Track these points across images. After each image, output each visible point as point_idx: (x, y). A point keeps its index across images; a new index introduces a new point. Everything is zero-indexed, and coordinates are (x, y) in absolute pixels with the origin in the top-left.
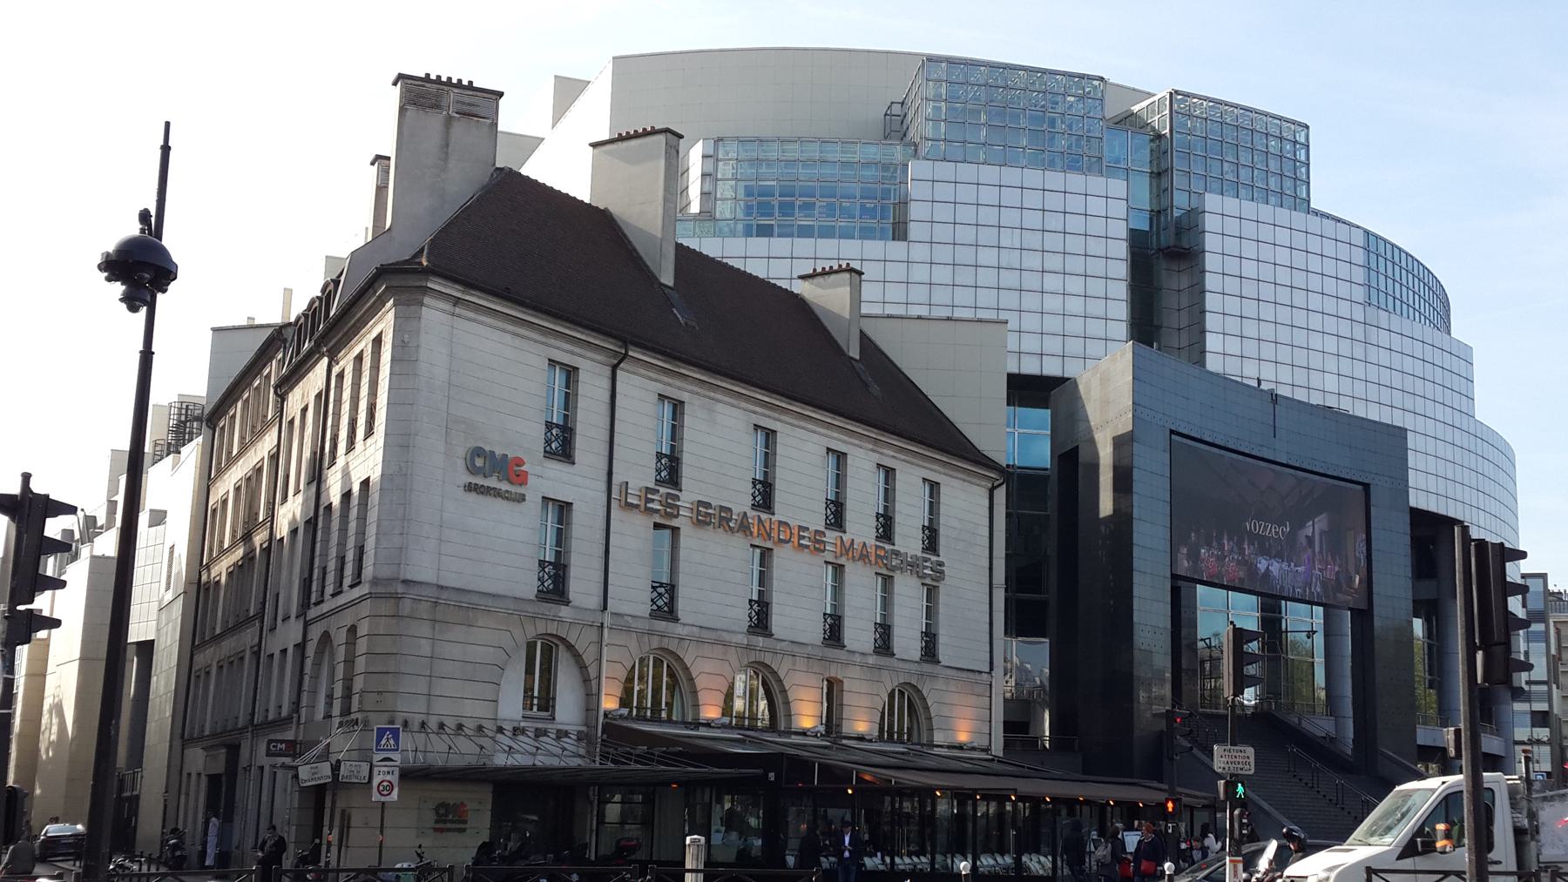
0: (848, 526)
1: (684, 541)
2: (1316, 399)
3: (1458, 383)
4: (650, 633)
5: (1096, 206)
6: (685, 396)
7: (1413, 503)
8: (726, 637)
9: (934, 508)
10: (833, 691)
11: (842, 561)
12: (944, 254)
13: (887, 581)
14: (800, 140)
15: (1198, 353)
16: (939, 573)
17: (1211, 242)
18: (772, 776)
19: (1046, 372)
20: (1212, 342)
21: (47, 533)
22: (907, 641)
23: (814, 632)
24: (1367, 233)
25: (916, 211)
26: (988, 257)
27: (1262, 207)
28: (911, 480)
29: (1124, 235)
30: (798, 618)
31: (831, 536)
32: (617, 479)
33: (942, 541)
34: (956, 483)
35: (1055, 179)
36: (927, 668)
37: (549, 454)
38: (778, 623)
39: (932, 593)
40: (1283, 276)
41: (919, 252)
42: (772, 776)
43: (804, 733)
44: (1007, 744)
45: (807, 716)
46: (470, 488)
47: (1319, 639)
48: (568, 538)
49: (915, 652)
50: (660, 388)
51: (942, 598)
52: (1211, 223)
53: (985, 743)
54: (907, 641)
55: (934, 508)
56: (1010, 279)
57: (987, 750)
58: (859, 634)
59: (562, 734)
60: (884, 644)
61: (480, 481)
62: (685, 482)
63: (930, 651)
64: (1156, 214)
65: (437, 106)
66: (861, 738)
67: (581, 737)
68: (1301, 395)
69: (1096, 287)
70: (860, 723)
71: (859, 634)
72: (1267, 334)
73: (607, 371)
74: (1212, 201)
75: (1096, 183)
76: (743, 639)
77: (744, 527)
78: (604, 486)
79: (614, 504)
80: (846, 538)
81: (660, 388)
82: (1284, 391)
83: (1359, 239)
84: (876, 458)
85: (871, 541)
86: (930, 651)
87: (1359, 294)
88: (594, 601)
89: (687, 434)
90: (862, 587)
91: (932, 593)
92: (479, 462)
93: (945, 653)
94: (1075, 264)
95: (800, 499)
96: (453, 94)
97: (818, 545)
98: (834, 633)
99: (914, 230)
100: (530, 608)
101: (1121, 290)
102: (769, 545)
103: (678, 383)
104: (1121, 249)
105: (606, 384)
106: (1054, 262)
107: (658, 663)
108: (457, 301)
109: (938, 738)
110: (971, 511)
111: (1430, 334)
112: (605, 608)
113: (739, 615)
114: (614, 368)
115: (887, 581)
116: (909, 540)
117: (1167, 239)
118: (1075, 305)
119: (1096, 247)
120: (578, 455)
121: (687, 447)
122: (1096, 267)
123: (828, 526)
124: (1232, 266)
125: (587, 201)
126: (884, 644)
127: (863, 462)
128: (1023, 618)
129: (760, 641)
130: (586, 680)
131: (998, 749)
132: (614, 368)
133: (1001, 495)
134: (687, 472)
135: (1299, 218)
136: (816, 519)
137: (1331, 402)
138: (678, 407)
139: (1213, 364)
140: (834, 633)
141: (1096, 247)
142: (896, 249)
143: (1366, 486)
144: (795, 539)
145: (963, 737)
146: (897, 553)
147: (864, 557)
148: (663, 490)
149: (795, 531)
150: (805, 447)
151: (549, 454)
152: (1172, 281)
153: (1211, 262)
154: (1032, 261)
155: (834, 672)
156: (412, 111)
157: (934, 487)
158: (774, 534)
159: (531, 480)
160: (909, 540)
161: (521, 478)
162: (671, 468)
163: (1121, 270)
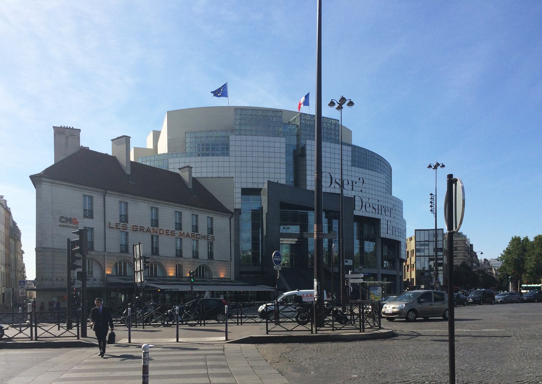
1: (129, 235)
5: (277, 145)
6: (128, 201)
11: (181, 237)
12: (238, 159)
14: (211, 131)
16: (213, 238)
19: (248, 187)
21: (352, 261)
22: (203, 253)
26: (250, 159)
31: (177, 232)
32: (107, 222)
33: (214, 231)
35: (271, 139)
36: (210, 261)
43: (170, 277)
46: (60, 226)
49: (206, 257)
50: (120, 200)
53: (229, 277)
56: (255, 164)
59: (95, 280)
61: (63, 224)
62: (129, 221)
63: (211, 256)
65: (64, 134)
67: (101, 280)
72: (333, 172)
73: (102, 196)
75: (277, 139)
77: (148, 230)
80: (182, 232)
84: (191, 212)
86: (211, 256)
88: (102, 250)
89: (129, 210)
92: (63, 220)
93: (215, 257)
94: (272, 160)
96: (67, 130)
99: (231, 154)
105: (102, 200)
106: (266, 160)
108: (52, 183)
109: (214, 276)
112: (105, 251)
118: (272, 170)
119: (277, 155)
120: (94, 216)
121: (129, 213)
122: (277, 160)
123: (176, 229)
125: (110, 154)
129: (155, 257)
130: (101, 268)
141: (277, 155)
142: (227, 158)
144: (165, 233)
145: (222, 276)
147: (188, 235)
148: (122, 224)
149: (165, 231)
154: (261, 159)
155: (179, 263)
156: (57, 133)
158: (158, 232)
159: (80, 223)
161: (77, 223)
162: (124, 218)
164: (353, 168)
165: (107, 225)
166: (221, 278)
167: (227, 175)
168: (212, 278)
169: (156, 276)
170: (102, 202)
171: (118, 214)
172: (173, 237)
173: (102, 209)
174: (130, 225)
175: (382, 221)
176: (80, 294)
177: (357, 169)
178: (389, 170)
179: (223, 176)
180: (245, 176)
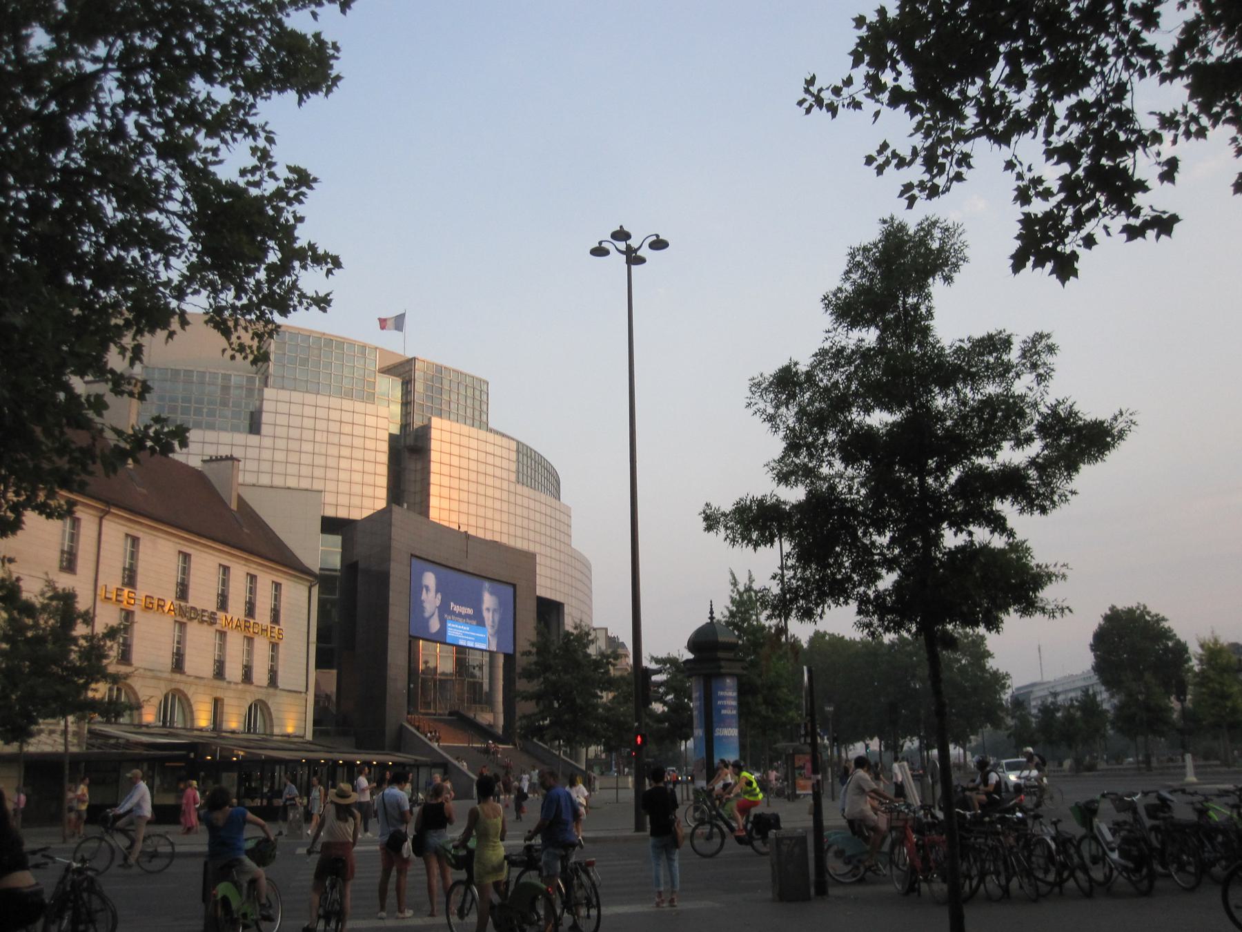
0: (230, 609)
2: (489, 537)
3: (564, 528)
4: (171, 681)
6: (140, 535)
7: (538, 593)
8: (159, 674)
9: (277, 598)
10: (217, 703)
13: (250, 640)
15: (424, 509)
17: (434, 445)
18: (192, 755)
20: (434, 501)
22: (260, 675)
23: (208, 670)
24: (518, 442)
25: (266, 418)
27: (463, 426)
28: (265, 580)
29: (386, 437)
30: (199, 661)
31: (221, 615)
32: (101, 583)
34: (290, 583)
36: (271, 690)
37: (62, 569)
38: (188, 666)
39: (274, 647)
40: (473, 466)
41: (267, 442)
42: (192, 755)
43: (201, 730)
44: (314, 732)
45: (203, 720)
47: (486, 669)
48: (185, 641)
50: (126, 530)
51: (281, 650)
52: (434, 434)
53: (302, 733)
54: (260, 675)
55: (277, 598)
57: (302, 737)
58: (234, 671)
60: (247, 677)
64: (405, 426)
66: (233, 732)
68: (481, 534)
69: (369, 467)
70: (233, 722)
71: (234, 671)
73: (97, 520)
74: (436, 422)
76: (167, 675)
78: (92, 587)
79: (98, 598)
81: (126, 530)
82: (472, 532)
83: (514, 446)
85: (242, 618)
87: (513, 477)
89: (141, 556)
90: (235, 642)
91: (274, 647)
95: (203, 596)
97: (213, 620)
98: (219, 673)
99: (265, 429)
100: (240, 687)
101: (383, 470)
102: (184, 620)
103: (137, 527)
104: (384, 447)
105: (307, 594)
107: (174, 696)
108: (246, 560)
109: (276, 731)
110: (299, 600)
111: (551, 500)
113: (167, 661)
114: (101, 519)
115: (250, 640)
116: (263, 615)
117: (410, 441)
124: (446, 459)
126: (247, 677)
127: (239, 572)
128: (324, 660)
129: (178, 677)
131: (309, 736)
132: (101, 519)
133: (315, 590)
134: (140, 579)
135: (483, 434)
136: (211, 606)
137: (497, 539)
138: (135, 541)
139: (434, 514)
140: (219, 673)
142: (253, 439)
143: (514, 586)
146: (193, 608)
149: (156, 602)
150: (206, 564)
151: (62, 569)
152: (411, 465)
153: (434, 456)
155: (219, 694)
157: (186, 557)
160: (263, 615)
163: (384, 458)
164: (519, 487)
165: (101, 592)
166: (288, 736)
167: (305, 484)
168: (272, 735)
169: (255, 732)
170: (95, 534)
171: (58, 548)
172: (212, 629)
173: (94, 550)
174: (141, 593)
175: (567, 609)
176: (1130, 763)
177: (526, 491)
178: (552, 479)
179: (309, 487)
180: (347, 490)
